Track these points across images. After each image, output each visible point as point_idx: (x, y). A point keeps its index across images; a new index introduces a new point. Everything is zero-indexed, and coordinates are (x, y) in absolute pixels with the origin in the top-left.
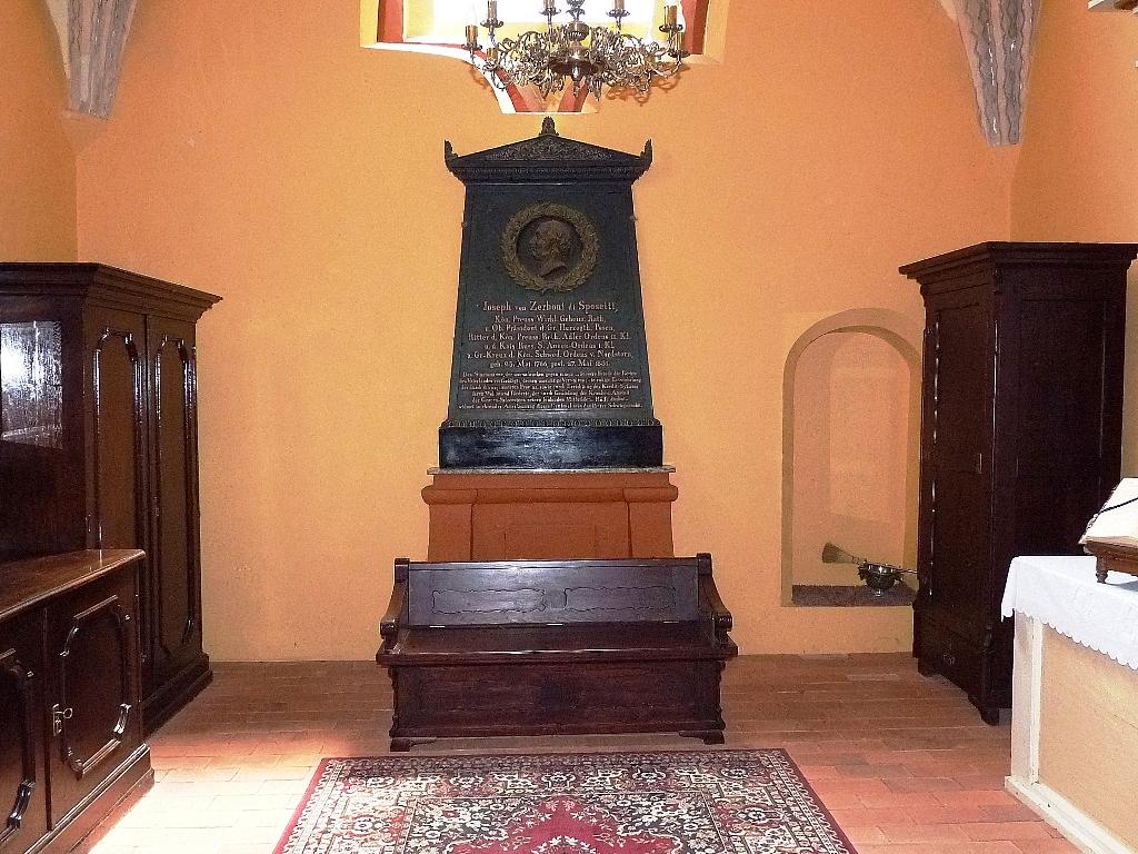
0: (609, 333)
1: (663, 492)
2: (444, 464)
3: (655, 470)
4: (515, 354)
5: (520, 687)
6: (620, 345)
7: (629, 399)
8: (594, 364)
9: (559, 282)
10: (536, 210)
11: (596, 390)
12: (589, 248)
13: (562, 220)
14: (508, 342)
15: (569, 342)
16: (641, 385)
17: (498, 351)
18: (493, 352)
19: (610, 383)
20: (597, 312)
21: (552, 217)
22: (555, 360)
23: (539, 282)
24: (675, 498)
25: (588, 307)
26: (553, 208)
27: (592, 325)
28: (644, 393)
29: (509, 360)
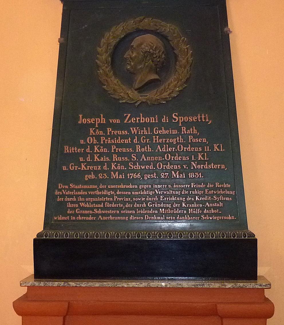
0: (202, 145)
1: (256, 308)
2: (39, 274)
3: (250, 285)
4: (109, 166)
5: (206, 178)
6: (212, 157)
7: (222, 211)
8: (187, 176)
9: (152, 95)
10: (131, 24)
11: (191, 202)
12: (182, 60)
13: (155, 33)
14: (101, 155)
15: (163, 154)
16: (234, 197)
17: (93, 163)
18: (89, 164)
19: (203, 195)
20: (188, 125)
21: (146, 31)
22: (149, 172)
23: (133, 94)
24: (270, 314)
25: (182, 119)
26: (147, 22)
27: (185, 137)
28: (244, 224)
29: (103, 171)
